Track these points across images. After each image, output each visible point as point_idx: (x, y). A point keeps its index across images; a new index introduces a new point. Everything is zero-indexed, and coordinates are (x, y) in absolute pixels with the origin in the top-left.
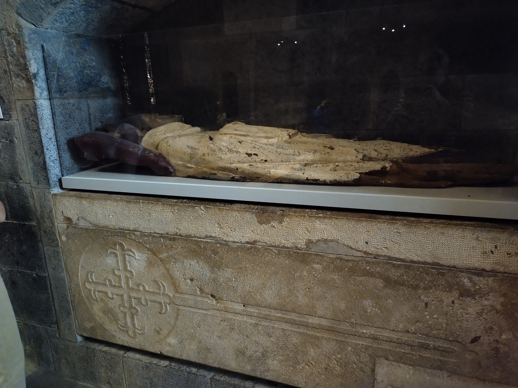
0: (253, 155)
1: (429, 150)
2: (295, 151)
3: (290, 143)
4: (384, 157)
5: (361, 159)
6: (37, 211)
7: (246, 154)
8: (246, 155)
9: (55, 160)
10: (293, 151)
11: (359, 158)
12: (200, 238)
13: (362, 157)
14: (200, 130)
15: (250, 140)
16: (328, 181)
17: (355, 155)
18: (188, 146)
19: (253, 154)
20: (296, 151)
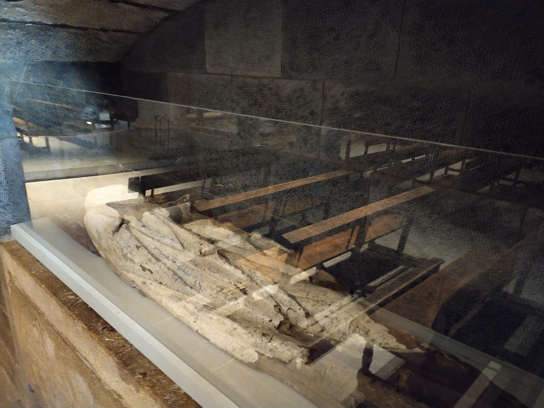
0: (147, 271)
1: (397, 344)
2: (196, 281)
3: (197, 265)
4: (317, 332)
5: (275, 327)
6: (137, 204)
7: (141, 266)
8: (140, 268)
9: (6, 205)
10: (194, 280)
11: (273, 325)
12: (81, 355)
13: (278, 323)
14: (143, 200)
15: (154, 245)
16: (218, 345)
17: (270, 317)
18: (97, 231)
19: (148, 269)
20: (198, 282)
